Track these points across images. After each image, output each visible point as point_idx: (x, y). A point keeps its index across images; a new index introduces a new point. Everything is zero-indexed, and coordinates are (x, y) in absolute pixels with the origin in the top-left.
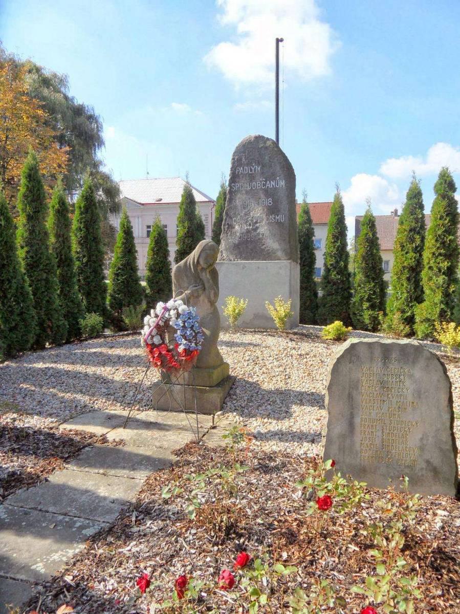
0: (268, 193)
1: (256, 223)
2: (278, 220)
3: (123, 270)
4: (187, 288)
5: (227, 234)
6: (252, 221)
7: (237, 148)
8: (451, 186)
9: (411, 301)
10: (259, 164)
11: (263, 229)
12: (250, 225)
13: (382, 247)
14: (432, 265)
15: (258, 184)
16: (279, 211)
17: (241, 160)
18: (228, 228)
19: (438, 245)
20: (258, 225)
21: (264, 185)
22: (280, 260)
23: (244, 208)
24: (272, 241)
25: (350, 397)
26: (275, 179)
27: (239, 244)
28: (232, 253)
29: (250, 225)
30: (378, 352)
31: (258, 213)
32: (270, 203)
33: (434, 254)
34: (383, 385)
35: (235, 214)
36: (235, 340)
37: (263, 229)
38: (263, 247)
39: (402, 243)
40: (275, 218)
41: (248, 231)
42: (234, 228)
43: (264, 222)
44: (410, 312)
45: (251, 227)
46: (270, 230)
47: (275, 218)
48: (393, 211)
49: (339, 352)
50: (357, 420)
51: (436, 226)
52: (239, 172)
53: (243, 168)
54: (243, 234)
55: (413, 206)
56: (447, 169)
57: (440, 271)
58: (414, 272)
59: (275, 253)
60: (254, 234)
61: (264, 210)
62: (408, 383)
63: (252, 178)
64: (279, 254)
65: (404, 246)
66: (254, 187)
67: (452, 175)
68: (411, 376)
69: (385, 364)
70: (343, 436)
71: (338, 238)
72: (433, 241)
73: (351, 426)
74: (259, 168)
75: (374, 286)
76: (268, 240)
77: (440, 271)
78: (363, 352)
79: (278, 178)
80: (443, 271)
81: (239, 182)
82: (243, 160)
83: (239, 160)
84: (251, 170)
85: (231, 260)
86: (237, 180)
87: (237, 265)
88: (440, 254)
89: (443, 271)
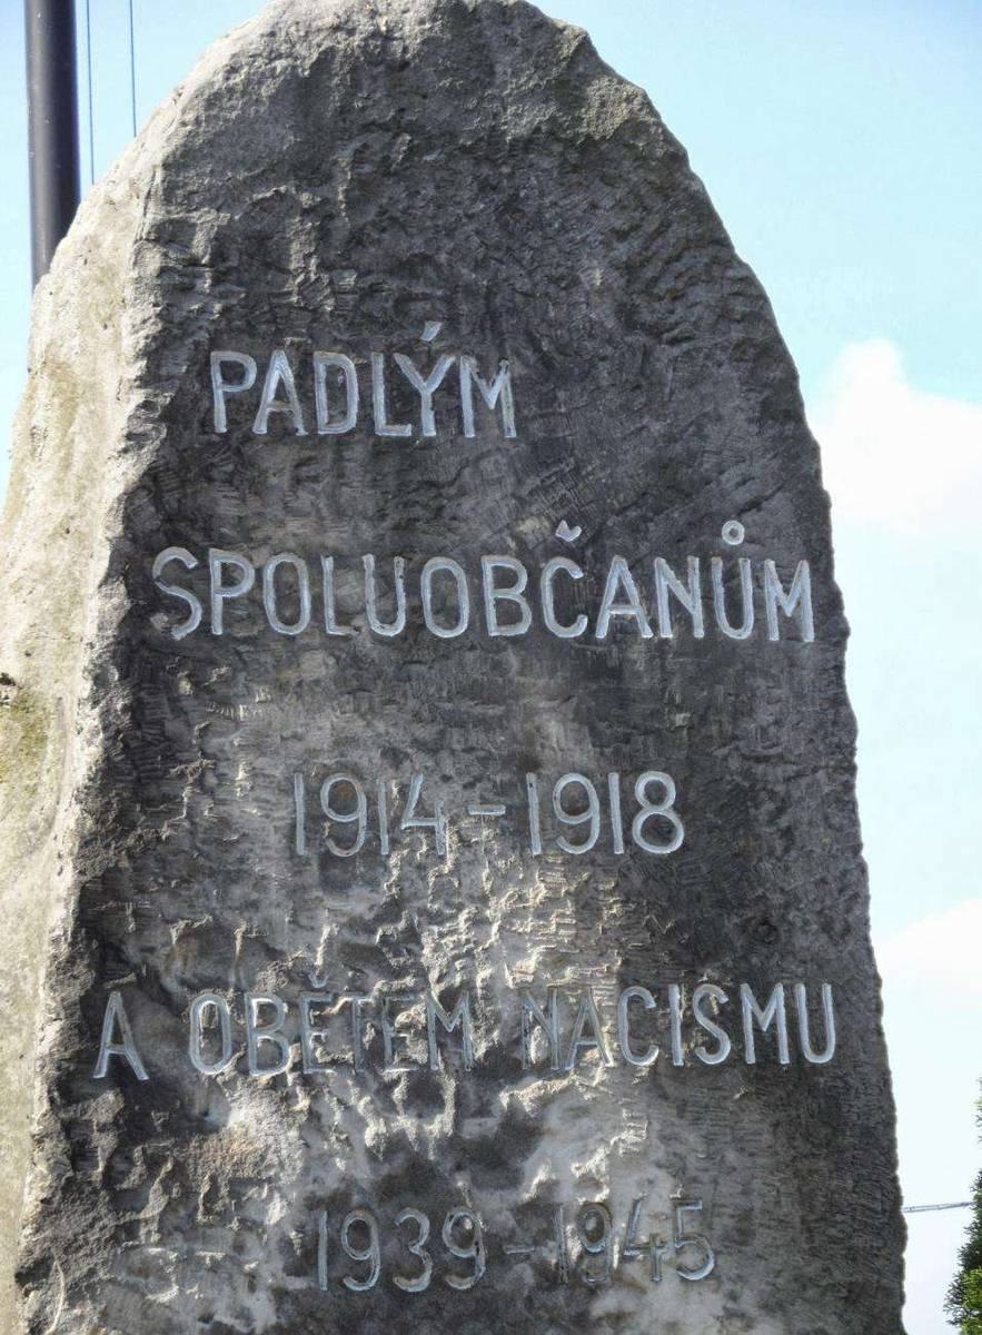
32: (659, 830)
47: (730, 1018)
52: (243, 408)
53: (304, 371)
74: (498, 390)
79: (733, 533)
81: (245, 538)
84: (404, 403)
86: (227, 506)
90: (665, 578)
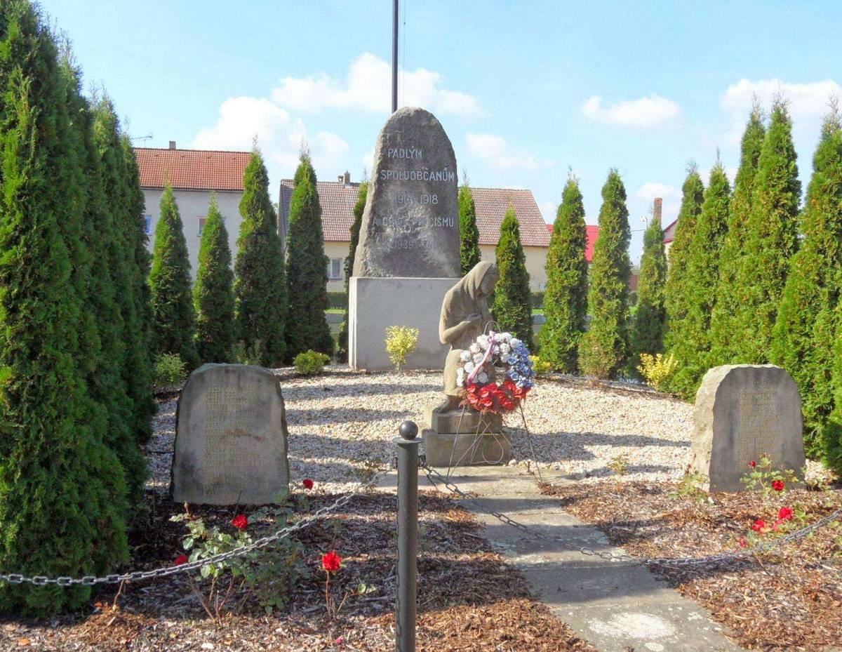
0: (432, 187)
1: (417, 226)
2: (445, 224)
3: (173, 284)
4: (464, 318)
5: (375, 239)
6: (411, 223)
7: (390, 121)
8: (622, 194)
9: (573, 331)
10: (419, 146)
11: (426, 235)
12: (407, 229)
13: (327, 236)
14: (605, 286)
15: (418, 174)
16: (446, 212)
17: (395, 138)
18: (376, 231)
19: (611, 262)
20: (419, 229)
21: (427, 176)
22: (446, 277)
23: (399, 205)
24: (437, 251)
25: (731, 415)
26: (440, 170)
27: (394, 253)
28: (381, 266)
29: (407, 229)
30: (751, 375)
31: (418, 213)
32: (435, 201)
33: (606, 272)
34: (755, 402)
35: (385, 211)
36: (386, 397)
37: (426, 235)
38: (425, 260)
39: (561, 257)
40: (441, 221)
41: (405, 237)
42: (384, 231)
43: (427, 226)
44: (573, 343)
45: (409, 231)
46: (435, 237)
47: (441, 221)
48: (343, 174)
49: (718, 377)
50: (736, 435)
51: (608, 240)
52: (392, 155)
53: (398, 151)
54: (398, 240)
55: (574, 212)
56: (617, 171)
57: (614, 294)
58: (577, 297)
59: (440, 268)
60: (414, 241)
61: (426, 209)
62: (773, 400)
63: (410, 164)
64: (447, 268)
65: (562, 261)
66: (413, 177)
67: (621, 179)
68: (775, 394)
69: (756, 385)
70: (724, 450)
71: (471, 245)
72: (605, 258)
73: (731, 441)
75: (522, 311)
76: (432, 250)
77: (614, 294)
78: (740, 376)
79: (445, 169)
80: (617, 294)
81: (391, 169)
82: (399, 139)
83: (392, 139)
84: (409, 154)
85: (380, 276)
86: (389, 165)
87: (389, 281)
88: (614, 274)
89: (617, 294)
90: (437, 174)
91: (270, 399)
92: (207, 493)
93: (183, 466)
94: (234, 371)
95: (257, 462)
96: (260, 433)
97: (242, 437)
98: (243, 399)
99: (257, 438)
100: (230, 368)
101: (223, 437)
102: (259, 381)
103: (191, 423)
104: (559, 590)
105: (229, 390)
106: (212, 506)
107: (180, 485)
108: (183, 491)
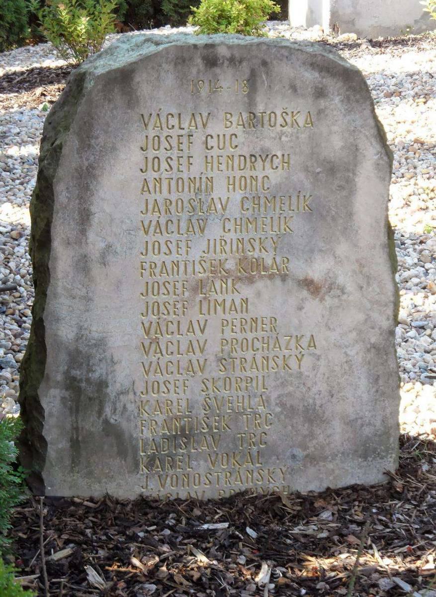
91: (354, 150)
92: (150, 464)
93: (72, 384)
94: (233, 61)
95: (307, 362)
96: (317, 270)
97: (260, 285)
98: (266, 156)
99: (308, 284)
100: (223, 51)
101: (200, 286)
102: (320, 93)
103: (95, 242)
104: (422, 113)
105: (216, 128)
106: (173, 505)
107: (64, 444)
108: (75, 461)
